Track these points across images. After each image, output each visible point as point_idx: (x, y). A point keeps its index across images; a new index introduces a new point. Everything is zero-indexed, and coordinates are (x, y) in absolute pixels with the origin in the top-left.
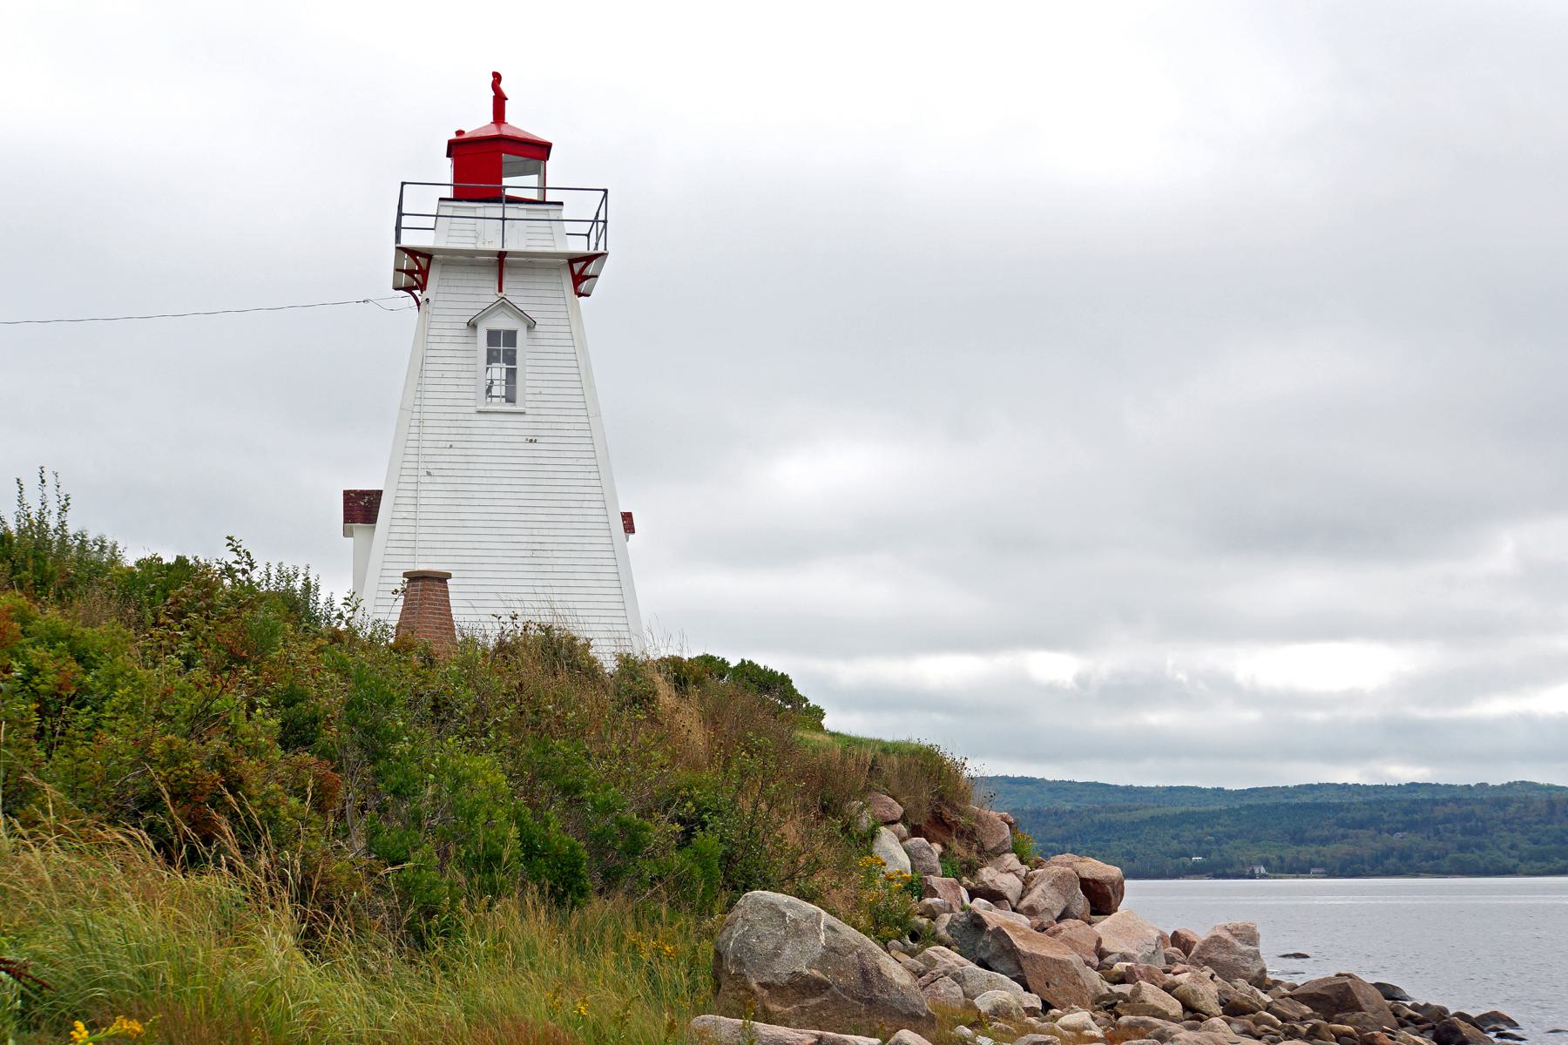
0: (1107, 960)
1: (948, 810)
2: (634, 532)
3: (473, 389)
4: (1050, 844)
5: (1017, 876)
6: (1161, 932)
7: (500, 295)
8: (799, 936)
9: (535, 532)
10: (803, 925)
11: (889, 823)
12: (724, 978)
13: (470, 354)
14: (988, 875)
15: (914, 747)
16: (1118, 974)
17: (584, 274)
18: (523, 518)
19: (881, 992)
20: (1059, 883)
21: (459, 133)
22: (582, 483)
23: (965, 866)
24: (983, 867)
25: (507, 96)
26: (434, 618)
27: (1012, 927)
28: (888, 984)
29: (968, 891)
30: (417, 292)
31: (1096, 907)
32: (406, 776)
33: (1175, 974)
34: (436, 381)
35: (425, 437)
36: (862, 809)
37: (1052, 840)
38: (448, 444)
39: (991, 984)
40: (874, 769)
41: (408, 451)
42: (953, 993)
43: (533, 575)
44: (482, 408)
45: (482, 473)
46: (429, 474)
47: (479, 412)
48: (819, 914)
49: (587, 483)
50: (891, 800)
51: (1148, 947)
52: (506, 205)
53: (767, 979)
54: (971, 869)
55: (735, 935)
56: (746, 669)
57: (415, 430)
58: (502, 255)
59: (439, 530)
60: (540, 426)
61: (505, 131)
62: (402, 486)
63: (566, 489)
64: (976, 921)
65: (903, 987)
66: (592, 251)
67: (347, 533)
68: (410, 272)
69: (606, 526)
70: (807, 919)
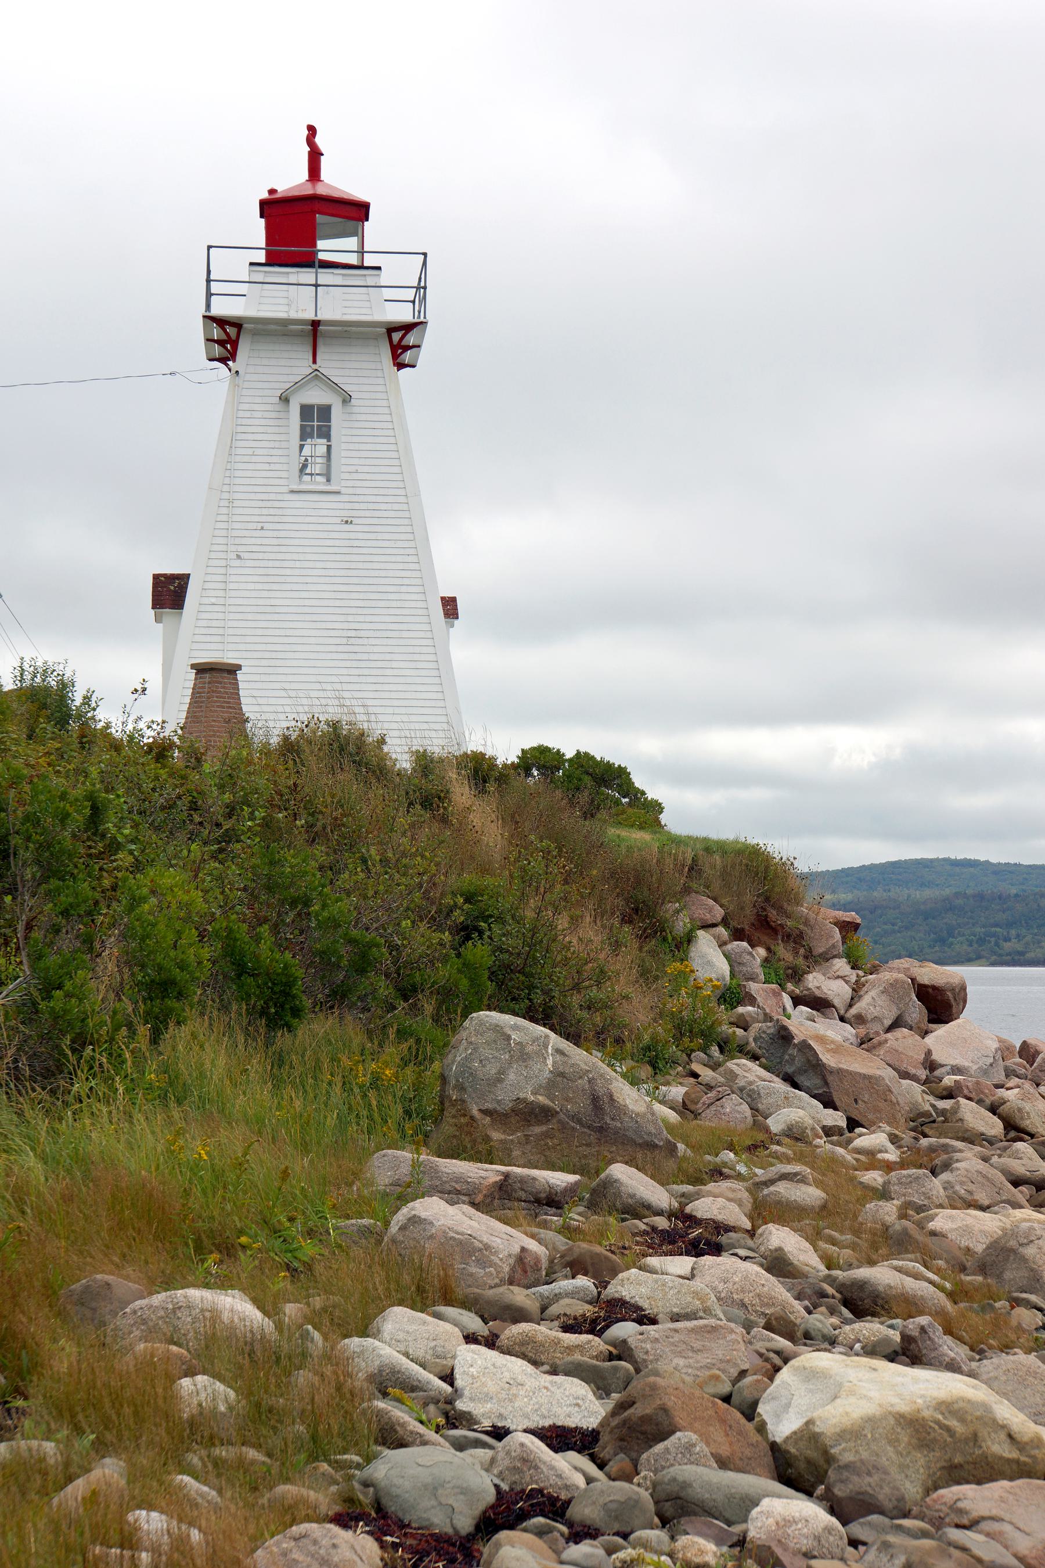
0: (937, 1073)
1: (775, 912)
2: (457, 618)
3: (285, 467)
4: (993, 929)
5: (847, 982)
6: (1000, 1041)
7: (315, 367)
8: (525, 1061)
9: (350, 618)
10: (529, 1049)
11: (707, 926)
12: (447, 1104)
13: (282, 430)
14: (816, 981)
15: (739, 846)
16: (946, 1089)
17: (404, 343)
18: (338, 603)
19: (613, 1119)
20: (891, 990)
21: (272, 191)
22: (401, 566)
23: (790, 971)
24: (809, 972)
25: (323, 150)
26: (223, 712)
27: (822, 1039)
28: (621, 1111)
29: (792, 998)
30: (230, 363)
31: (936, 1013)
32: (77, 897)
33: (1008, 1089)
34: (246, 459)
35: (235, 518)
36: (678, 912)
37: (996, 925)
38: (259, 526)
39: (787, 1101)
40: (694, 869)
41: (217, 533)
42: (739, 1112)
43: (348, 664)
44: (295, 487)
45: (295, 557)
46: (239, 557)
47: (292, 492)
48: (547, 1036)
49: (406, 566)
50: (711, 902)
51: (985, 1059)
52: (320, 270)
53: (488, 1106)
54: (796, 975)
55: (458, 1059)
56: (583, 760)
57: (225, 511)
58: (315, 324)
59: (250, 617)
60: (356, 506)
61: (321, 190)
62: (210, 570)
63: (383, 573)
64: (783, 1033)
65: (637, 1115)
66: (416, 320)
67: (158, 619)
68: (221, 343)
69: (424, 612)
70: (534, 1042)
